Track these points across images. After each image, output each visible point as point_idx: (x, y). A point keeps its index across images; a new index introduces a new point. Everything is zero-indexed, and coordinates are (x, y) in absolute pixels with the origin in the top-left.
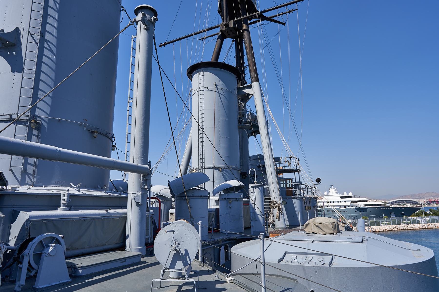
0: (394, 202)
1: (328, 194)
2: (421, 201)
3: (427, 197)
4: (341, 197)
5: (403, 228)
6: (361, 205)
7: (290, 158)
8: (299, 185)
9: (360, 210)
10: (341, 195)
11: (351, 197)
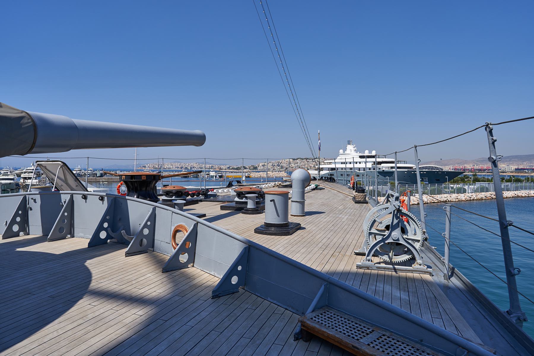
1: (344, 152)
4: (361, 157)
5: (445, 199)
6: (386, 167)
9: (384, 174)
10: (361, 154)
11: (373, 157)
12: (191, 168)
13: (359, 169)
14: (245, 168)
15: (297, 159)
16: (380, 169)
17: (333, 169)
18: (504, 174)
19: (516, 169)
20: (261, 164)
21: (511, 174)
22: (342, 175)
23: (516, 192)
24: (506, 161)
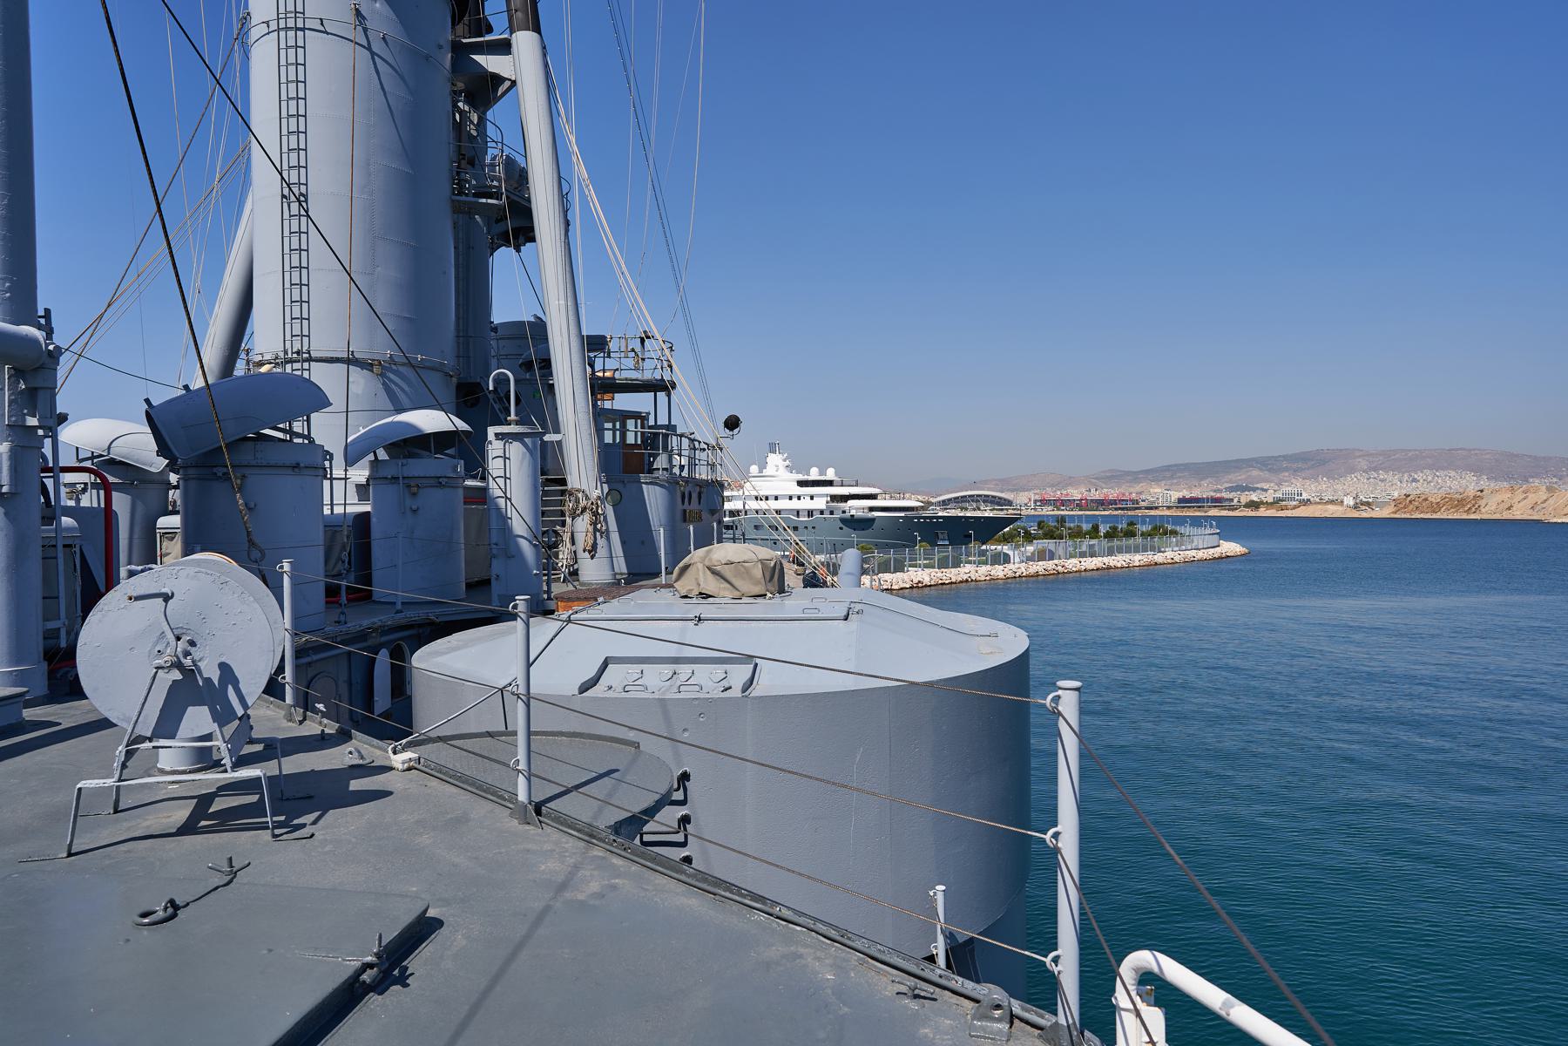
4: (801, 484)
7: (642, 341)
8: (666, 436)
10: (801, 477)
11: (830, 483)
13: (798, 513)
18: (1153, 513)
19: (1180, 500)
21: (1168, 513)
22: (756, 527)
23: (1106, 560)
24: (1164, 478)
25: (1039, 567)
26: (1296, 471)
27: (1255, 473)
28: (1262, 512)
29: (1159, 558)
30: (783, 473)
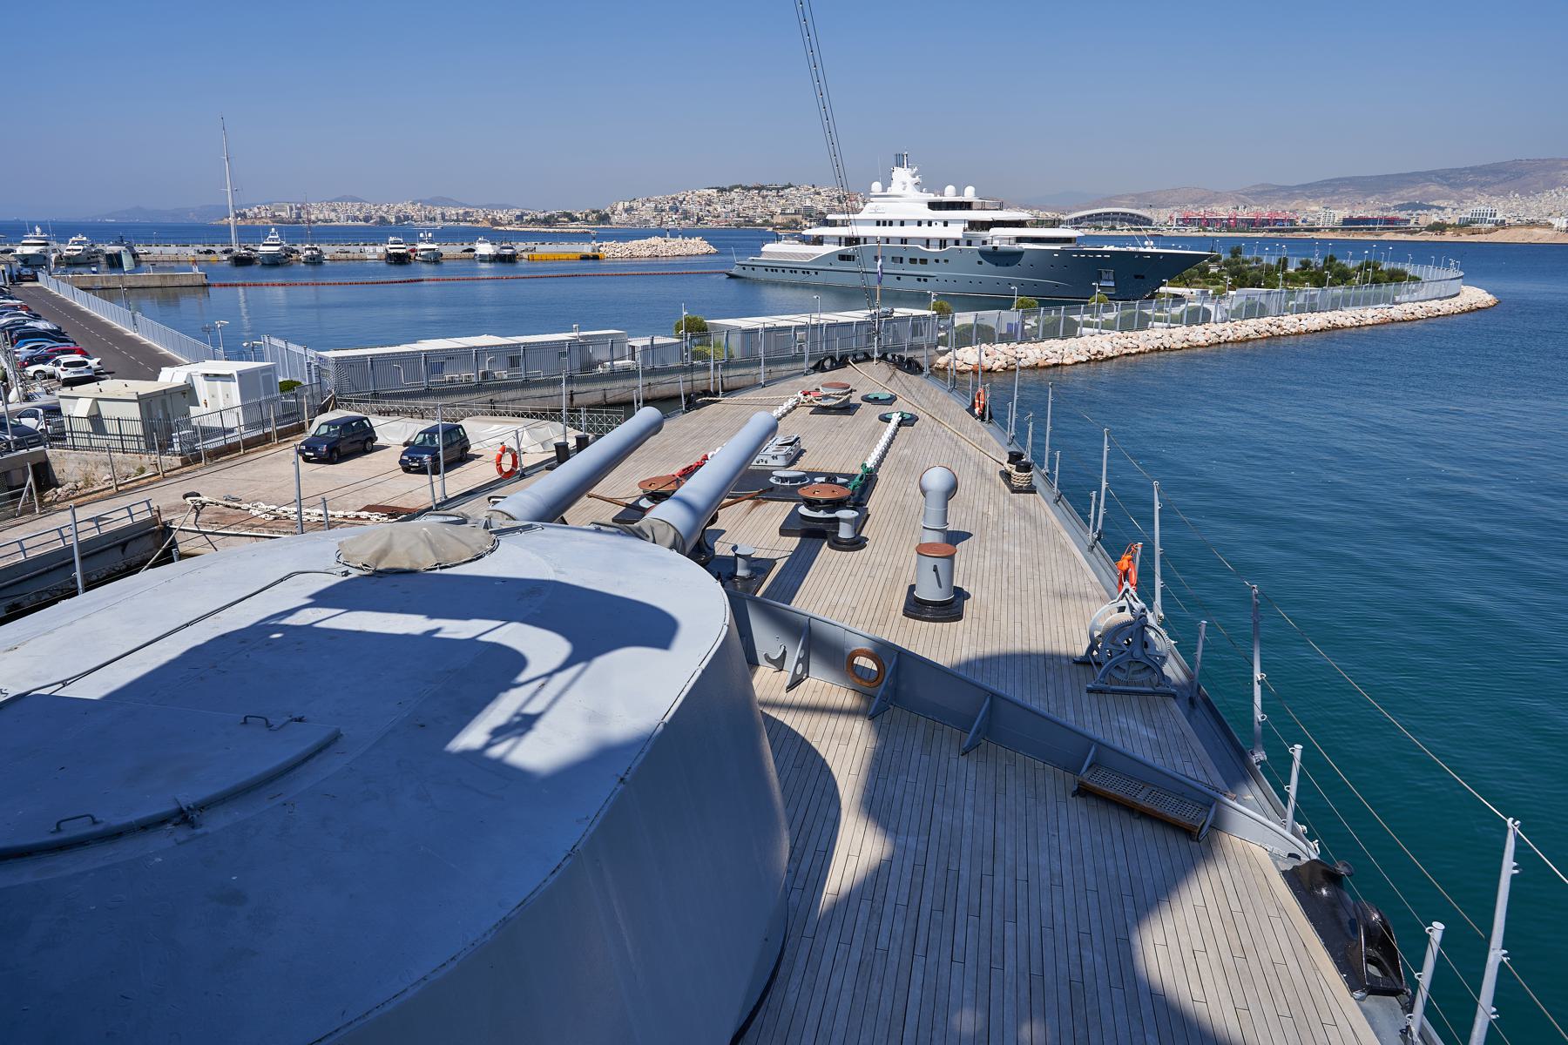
0: (1082, 218)
1: (884, 190)
2: (1159, 216)
3: (1178, 204)
4: (933, 206)
5: (1157, 344)
6: (1001, 239)
9: (997, 257)
10: (932, 197)
11: (967, 206)
12: (398, 218)
13: (928, 242)
14: (573, 219)
15: (731, 189)
16: (984, 243)
17: (851, 241)
18: (1315, 235)
19: (1346, 221)
20: (620, 207)
21: (1331, 236)
24: (1324, 195)
25: (1249, 327)
26: (1482, 187)
27: (1433, 188)
28: (1449, 236)
29: (1396, 312)
30: (912, 192)
